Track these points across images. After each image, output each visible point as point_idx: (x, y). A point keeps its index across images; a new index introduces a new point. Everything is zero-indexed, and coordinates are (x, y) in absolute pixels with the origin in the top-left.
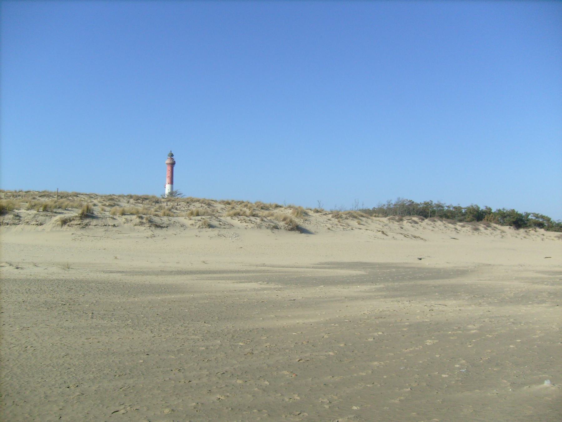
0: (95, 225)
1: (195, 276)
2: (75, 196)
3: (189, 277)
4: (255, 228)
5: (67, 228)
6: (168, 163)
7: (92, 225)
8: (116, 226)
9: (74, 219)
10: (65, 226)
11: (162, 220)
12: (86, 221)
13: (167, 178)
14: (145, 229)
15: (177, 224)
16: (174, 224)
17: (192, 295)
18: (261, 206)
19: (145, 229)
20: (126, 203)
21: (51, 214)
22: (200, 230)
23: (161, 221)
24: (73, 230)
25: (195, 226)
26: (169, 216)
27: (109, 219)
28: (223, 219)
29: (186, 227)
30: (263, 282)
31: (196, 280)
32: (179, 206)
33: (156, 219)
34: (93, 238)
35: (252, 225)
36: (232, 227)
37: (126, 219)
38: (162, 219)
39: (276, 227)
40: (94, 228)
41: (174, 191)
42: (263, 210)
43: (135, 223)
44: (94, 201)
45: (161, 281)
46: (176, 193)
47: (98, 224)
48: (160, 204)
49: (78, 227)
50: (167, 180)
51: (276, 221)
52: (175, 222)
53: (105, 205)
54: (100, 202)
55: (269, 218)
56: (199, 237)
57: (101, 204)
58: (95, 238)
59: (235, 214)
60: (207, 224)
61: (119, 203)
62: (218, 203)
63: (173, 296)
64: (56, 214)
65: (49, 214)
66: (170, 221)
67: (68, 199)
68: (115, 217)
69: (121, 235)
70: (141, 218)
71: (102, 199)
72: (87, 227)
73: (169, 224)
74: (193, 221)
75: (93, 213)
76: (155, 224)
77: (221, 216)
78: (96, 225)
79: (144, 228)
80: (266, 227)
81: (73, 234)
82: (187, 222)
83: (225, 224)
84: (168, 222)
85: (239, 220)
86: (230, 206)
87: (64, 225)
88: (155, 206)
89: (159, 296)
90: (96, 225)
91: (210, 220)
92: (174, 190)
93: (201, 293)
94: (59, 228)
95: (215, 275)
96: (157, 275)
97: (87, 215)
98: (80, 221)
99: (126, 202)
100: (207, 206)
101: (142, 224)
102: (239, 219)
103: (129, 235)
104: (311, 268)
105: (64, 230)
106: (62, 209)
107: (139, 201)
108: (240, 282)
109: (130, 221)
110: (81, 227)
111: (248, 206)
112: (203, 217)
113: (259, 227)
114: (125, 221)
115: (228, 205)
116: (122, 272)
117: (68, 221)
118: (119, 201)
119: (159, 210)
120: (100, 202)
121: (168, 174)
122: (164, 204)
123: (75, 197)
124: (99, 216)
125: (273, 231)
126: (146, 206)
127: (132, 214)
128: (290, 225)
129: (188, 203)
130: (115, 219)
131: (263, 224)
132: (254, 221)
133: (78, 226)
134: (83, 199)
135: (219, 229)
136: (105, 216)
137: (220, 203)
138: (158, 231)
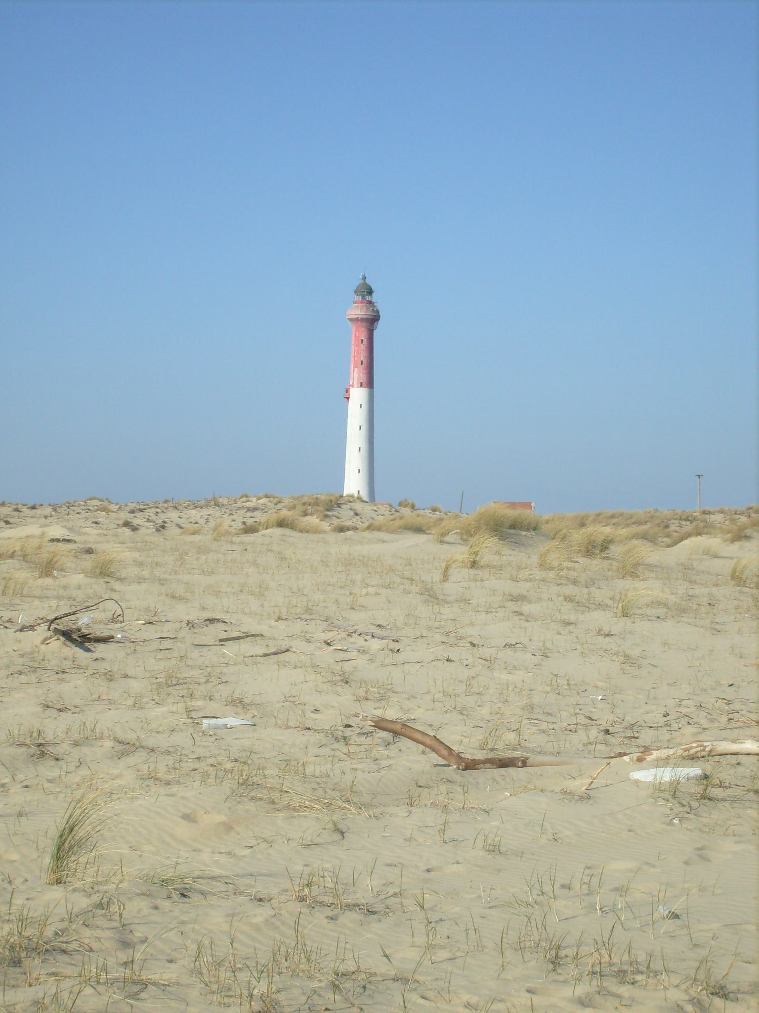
6: (360, 317)
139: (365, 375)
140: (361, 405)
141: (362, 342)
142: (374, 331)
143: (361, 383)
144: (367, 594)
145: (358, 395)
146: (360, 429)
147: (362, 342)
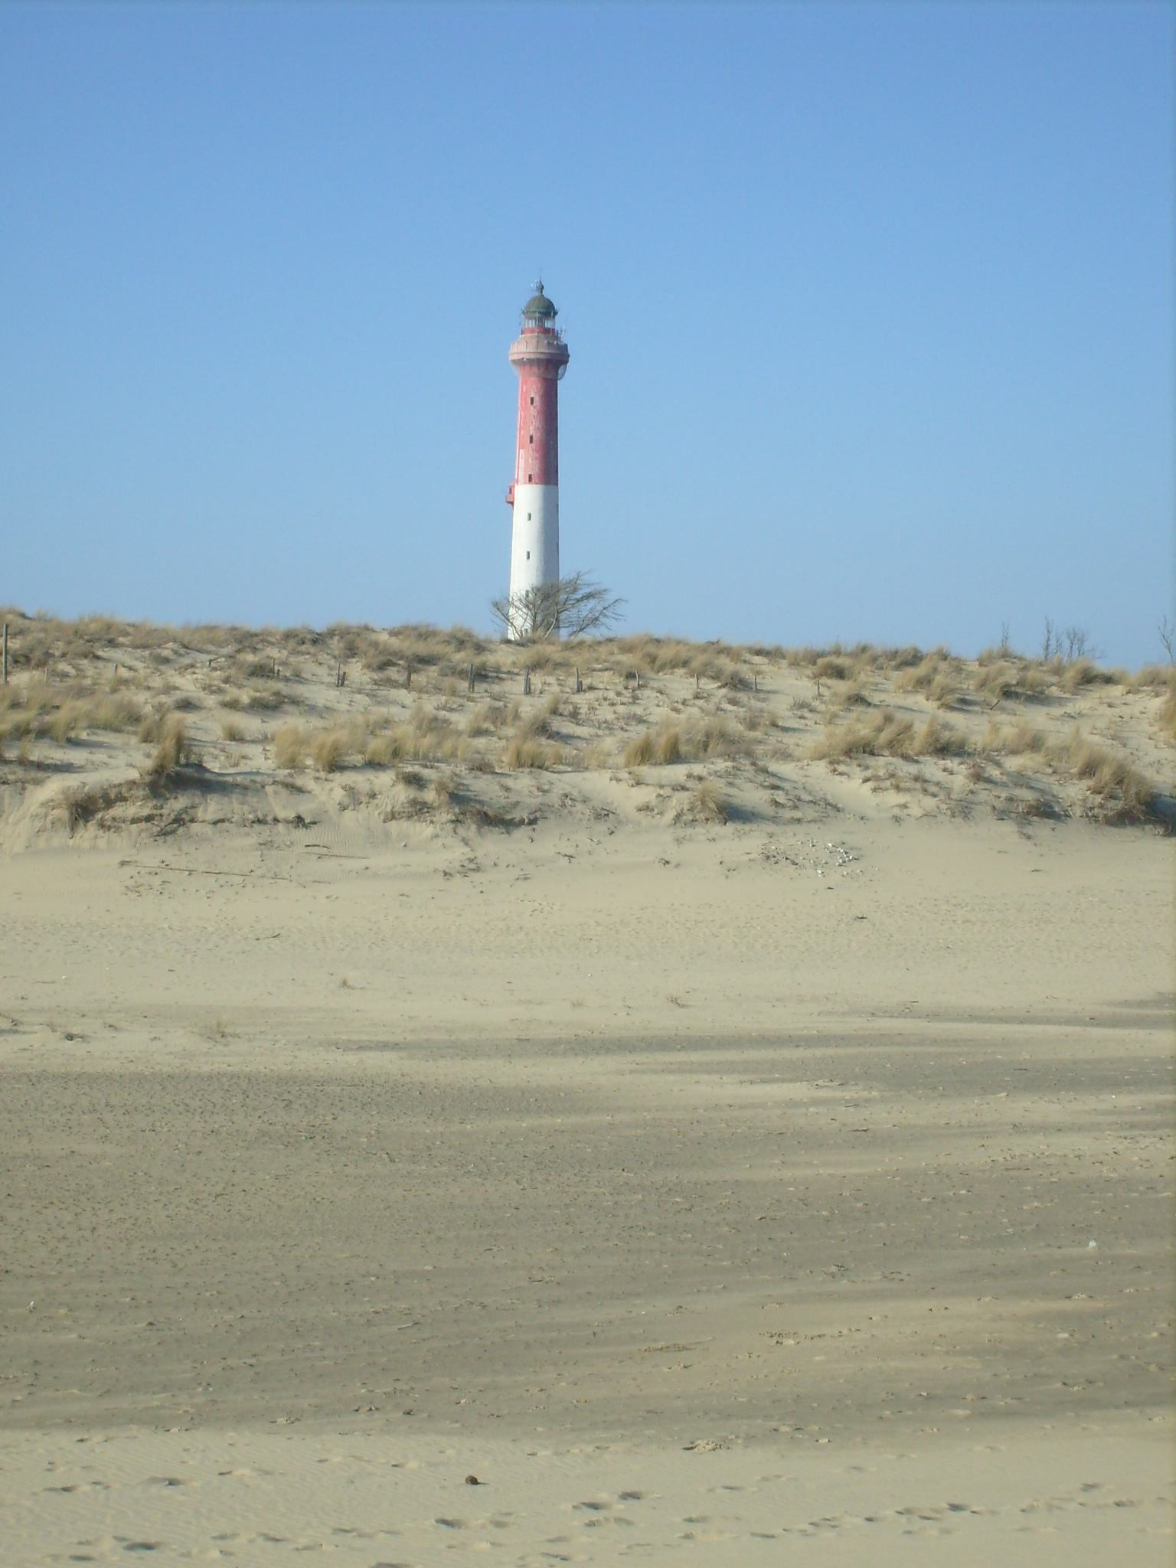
0: (215, 823)
1: (630, 1057)
2: (86, 657)
3: (611, 1062)
4: (941, 818)
5: (96, 837)
6: (526, 357)
7: (203, 822)
8: (307, 821)
9: (126, 795)
10: (85, 826)
11: (508, 789)
12: (178, 803)
13: (522, 447)
14: (437, 836)
15: (579, 807)
16: (564, 805)
17: (609, 1118)
18: (1001, 680)
19: (437, 836)
20: (328, 685)
21: (20, 773)
22: (680, 832)
23: (502, 793)
24: (122, 844)
25: (661, 813)
26: (540, 767)
27: (276, 793)
28: (794, 777)
29: (620, 822)
30: (831, 1081)
31: (631, 1072)
32: (590, 696)
33: (484, 787)
34: (212, 879)
35: (929, 803)
36: (832, 813)
37: (351, 791)
38: (509, 782)
39: (1046, 811)
40: (210, 833)
41: (561, 578)
42: (1009, 704)
43: (389, 809)
44: (177, 680)
45: (524, 1077)
46: (575, 590)
47: (229, 816)
48: (496, 688)
49: (142, 830)
50: (522, 462)
51: (1051, 783)
52: (567, 796)
53: (233, 705)
54: (208, 688)
55: (1013, 763)
56: (677, 866)
57: (213, 697)
58: (221, 882)
59: (851, 750)
60: (712, 806)
61: (299, 690)
62: (784, 663)
63: (560, 1120)
64: (40, 775)
65: (14, 773)
66: (544, 791)
67: (54, 673)
68: (299, 781)
69: (330, 865)
70: (415, 781)
71: (215, 669)
72: (181, 830)
73: (540, 810)
74: (651, 788)
75: (200, 766)
76: (479, 813)
77: (785, 756)
78: (222, 821)
79: (428, 830)
80: (994, 808)
81: (123, 863)
82: (626, 797)
83: (797, 803)
84: (536, 801)
85: (866, 780)
86: (843, 687)
87: (81, 823)
88: (470, 699)
89: (523, 1121)
90: (222, 821)
91: (730, 784)
92: (565, 573)
93: (635, 1111)
94: (61, 838)
95: (696, 1057)
96: (509, 1055)
97: (178, 774)
98: (150, 804)
99: (328, 679)
100: (724, 691)
101: (419, 810)
102: (868, 773)
103: (365, 863)
104: (1086, 1025)
105: (86, 845)
106: (52, 738)
107: (392, 673)
108: (763, 1081)
109: (365, 799)
110: (156, 829)
111: (935, 684)
112: (698, 769)
113: (964, 810)
114: (347, 801)
115: (829, 682)
116: (395, 1046)
117: (101, 803)
118: (298, 677)
119: (492, 728)
120: (210, 686)
121: (527, 421)
122: (514, 687)
123: (85, 662)
124: (230, 779)
125: (1029, 830)
126: (430, 705)
127: (374, 765)
128: (1112, 797)
129: (630, 676)
130: (300, 790)
131: (983, 796)
132: (938, 784)
133: (143, 825)
134: (124, 673)
135: (771, 828)
136: (253, 778)
137: (795, 663)
138: (493, 845)
139: (537, 461)
140: (528, 553)
141: (532, 403)
142: (558, 382)
143: (530, 476)
144: (352, 1154)
145: (527, 497)
146: (528, 557)
147: (532, 403)
